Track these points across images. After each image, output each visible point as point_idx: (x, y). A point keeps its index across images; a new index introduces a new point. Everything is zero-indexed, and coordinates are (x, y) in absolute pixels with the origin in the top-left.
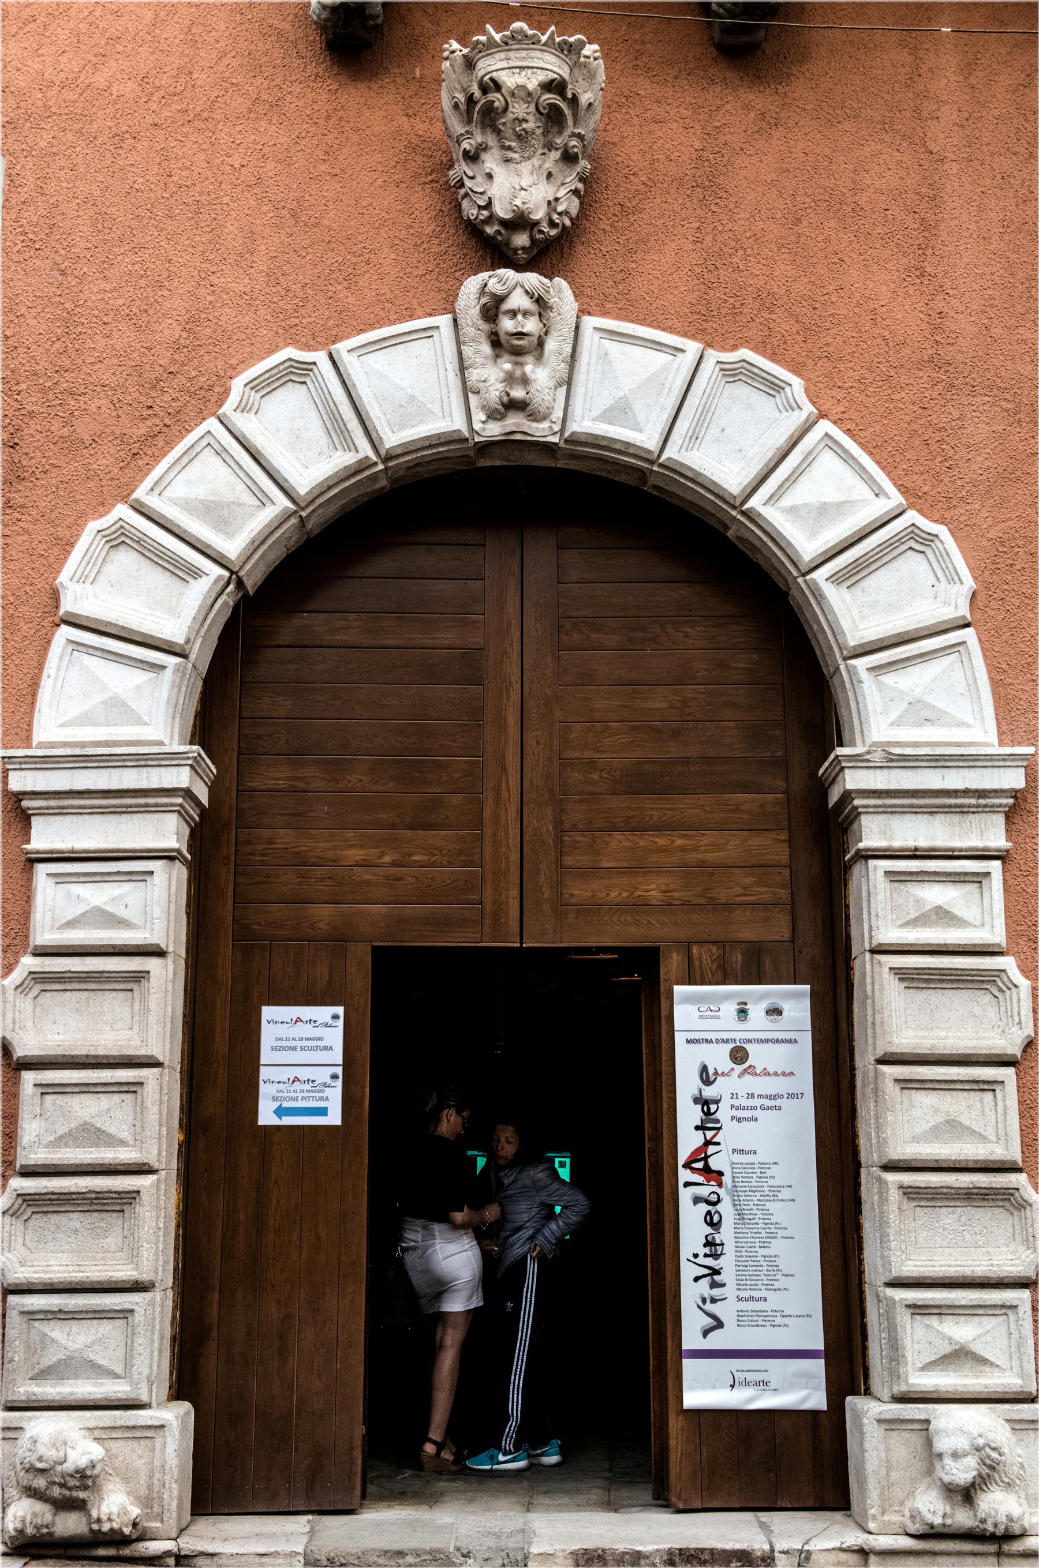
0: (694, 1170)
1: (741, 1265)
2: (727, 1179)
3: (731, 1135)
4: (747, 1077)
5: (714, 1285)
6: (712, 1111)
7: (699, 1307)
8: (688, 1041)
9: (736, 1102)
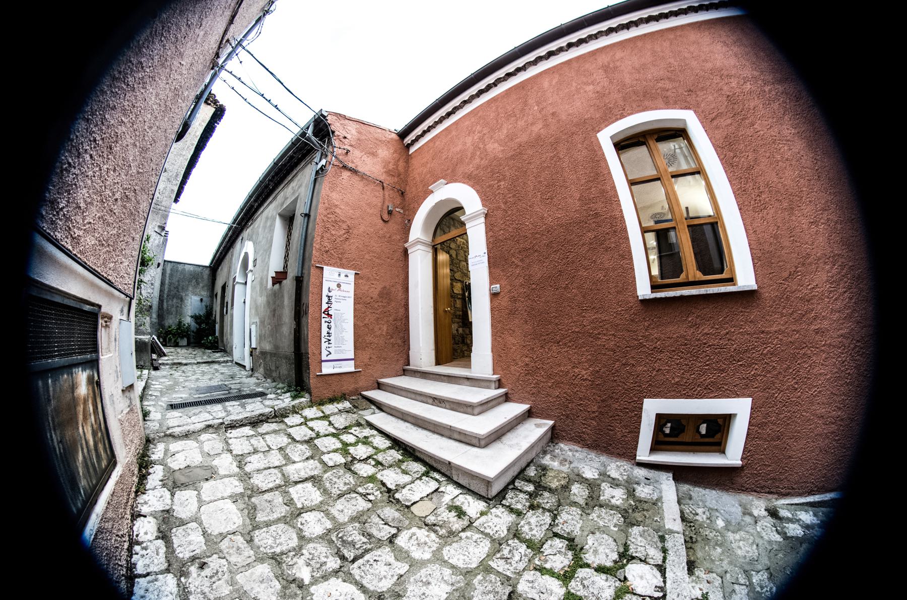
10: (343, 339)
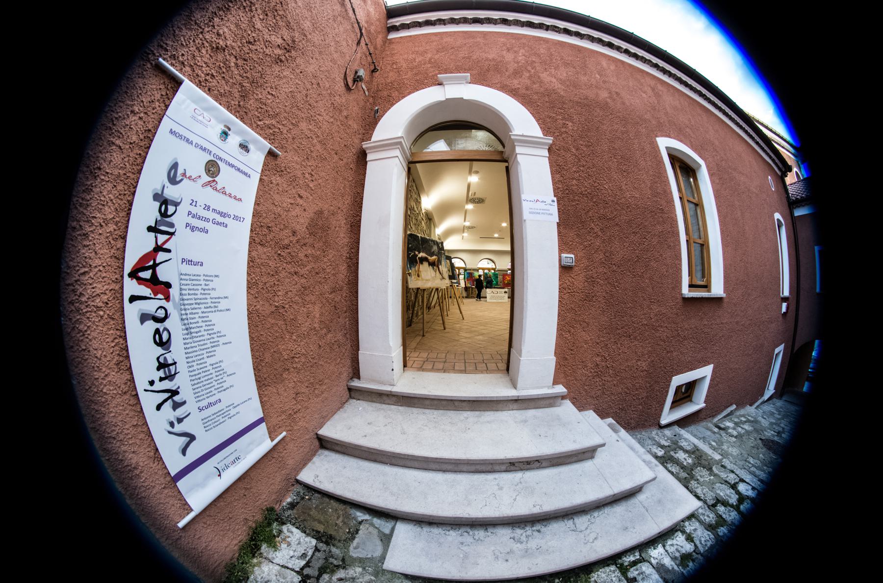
0: (141, 281)
1: (195, 380)
2: (174, 292)
3: (182, 243)
4: (209, 188)
5: (176, 406)
6: (169, 213)
7: (170, 433)
8: (171, 132)
9: (194, 210)
10: (220, 372)
